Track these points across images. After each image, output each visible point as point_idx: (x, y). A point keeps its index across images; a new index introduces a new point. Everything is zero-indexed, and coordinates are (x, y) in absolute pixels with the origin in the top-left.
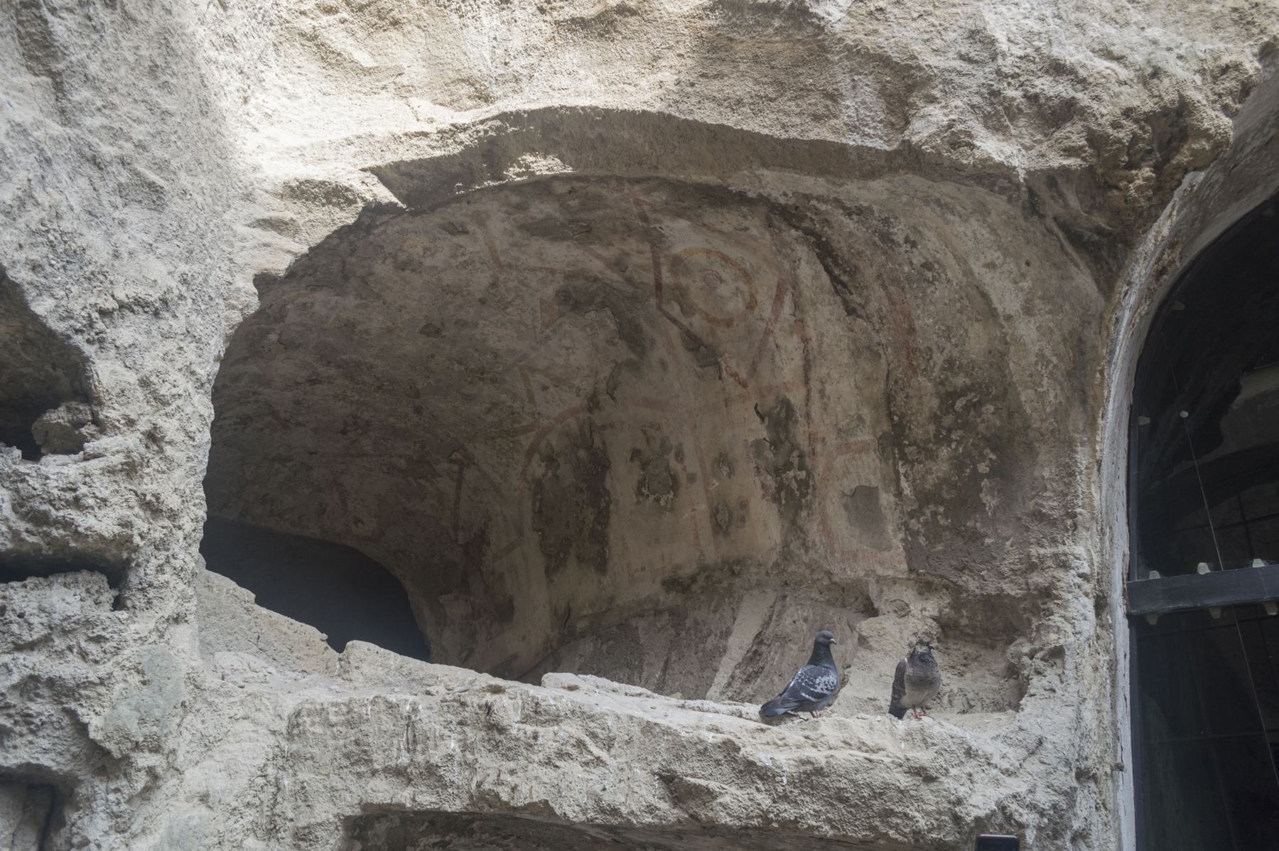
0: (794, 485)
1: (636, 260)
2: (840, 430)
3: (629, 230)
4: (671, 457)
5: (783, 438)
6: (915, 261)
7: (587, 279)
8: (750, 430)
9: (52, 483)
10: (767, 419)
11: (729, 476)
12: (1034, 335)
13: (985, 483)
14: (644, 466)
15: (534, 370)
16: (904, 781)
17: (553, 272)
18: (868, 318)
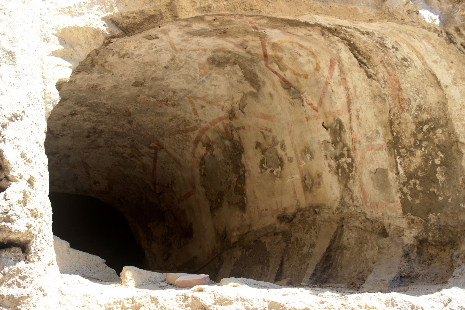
0: (346, 166)
1: (252, 43)
2: (368, 138)
3: (247, 32)
4: (278, 147)
5: (338, 140)
6: (398, 57)
7: (225, 52)
8: (321, 135)
10: (329, 129)
11: (312, 158)
12: (459, 95)
14: (263, 152)
15: (196, 98)
17: (205, 50)
18: (378, 81)
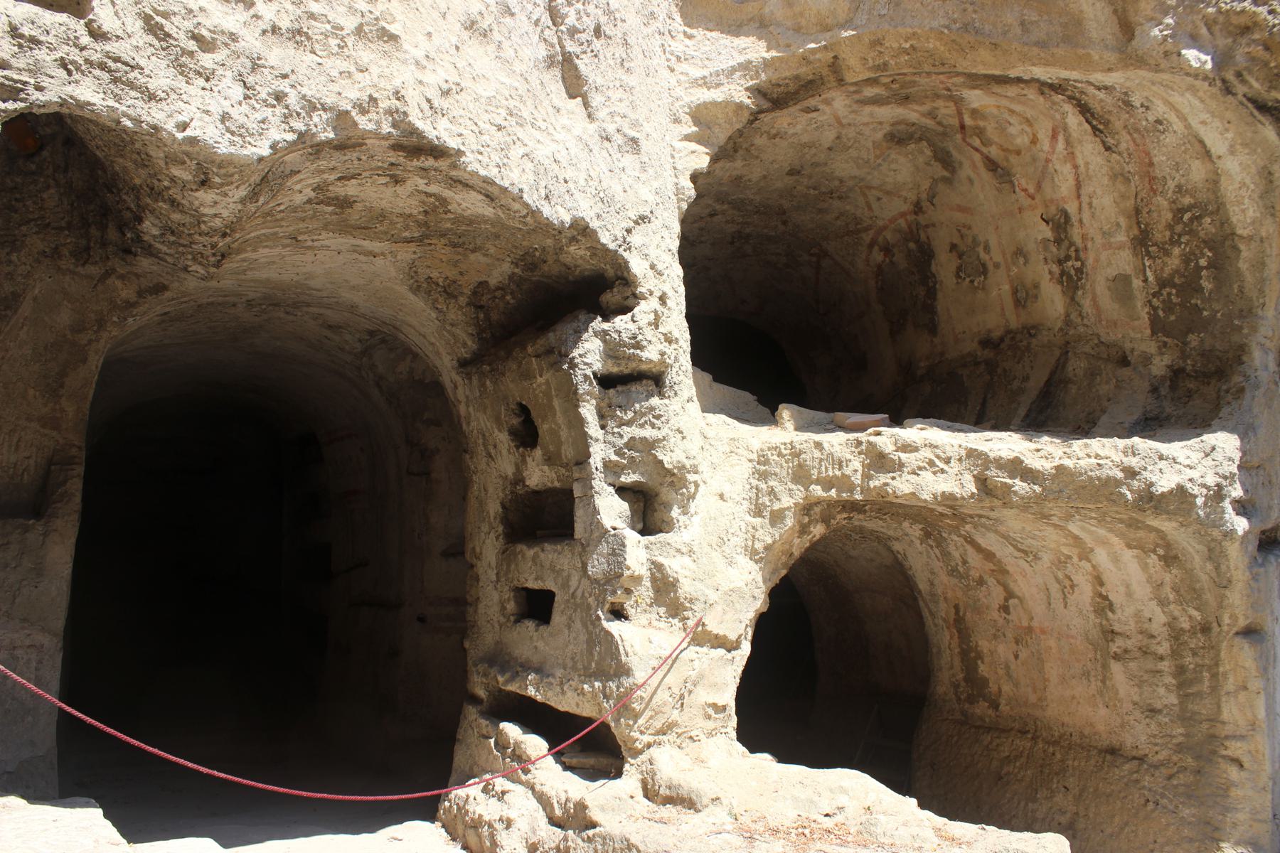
0: (1073, 272)
1: (943, 111)
3: (937, 96)
4: (980, 250)
9: (623, 335)
12: (1238, 169)
13: (1204, 273)
14: (960, 256)
15: (869, 188)
16: (1120, 475)
17: (881, 123)
18: (1120, 154)
